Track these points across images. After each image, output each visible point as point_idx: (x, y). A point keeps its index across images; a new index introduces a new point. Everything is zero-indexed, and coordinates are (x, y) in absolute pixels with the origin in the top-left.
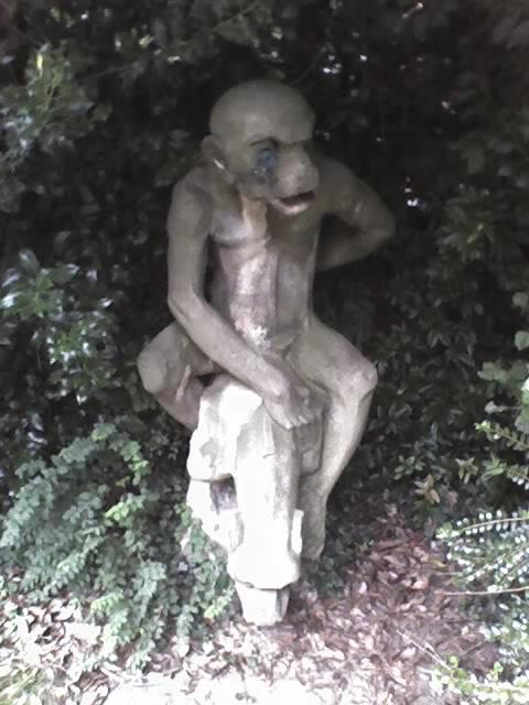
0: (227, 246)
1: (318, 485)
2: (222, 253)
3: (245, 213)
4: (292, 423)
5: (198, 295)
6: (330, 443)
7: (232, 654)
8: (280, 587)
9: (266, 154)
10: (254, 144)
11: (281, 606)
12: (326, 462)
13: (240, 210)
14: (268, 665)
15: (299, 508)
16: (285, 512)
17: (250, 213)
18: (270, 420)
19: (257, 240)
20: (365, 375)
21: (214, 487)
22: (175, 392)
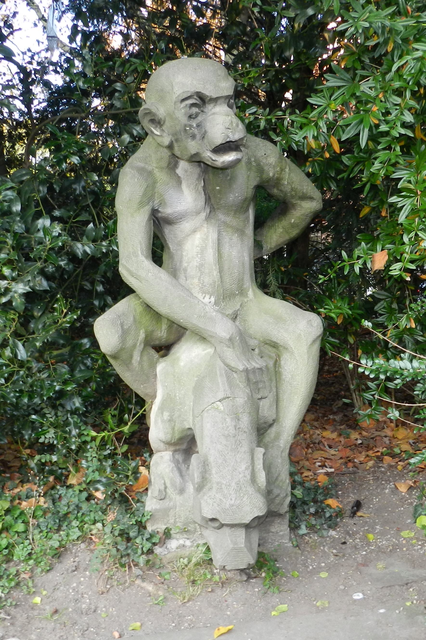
0: (169, 221)
1: (277, 437)
2: (167, 231)
3: (184, 186)
4: (244, 365)
5: (146, 257)
6: (285, 397)
7: (145, 531)
8: (247, 520)
9: (195, 110)
10: (183, 100)
11: (251, 545)
12: (284, 403)
13: (179, 181)
14: (216, 49)
15: (259, 446)
16: (245, 447)
17: (189, 187)
18: (222, 365)
19: (198, 213)
20: (309, 322)
21: (177, 456)
22: (131, 357)
